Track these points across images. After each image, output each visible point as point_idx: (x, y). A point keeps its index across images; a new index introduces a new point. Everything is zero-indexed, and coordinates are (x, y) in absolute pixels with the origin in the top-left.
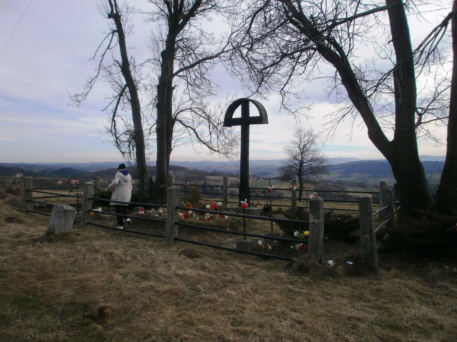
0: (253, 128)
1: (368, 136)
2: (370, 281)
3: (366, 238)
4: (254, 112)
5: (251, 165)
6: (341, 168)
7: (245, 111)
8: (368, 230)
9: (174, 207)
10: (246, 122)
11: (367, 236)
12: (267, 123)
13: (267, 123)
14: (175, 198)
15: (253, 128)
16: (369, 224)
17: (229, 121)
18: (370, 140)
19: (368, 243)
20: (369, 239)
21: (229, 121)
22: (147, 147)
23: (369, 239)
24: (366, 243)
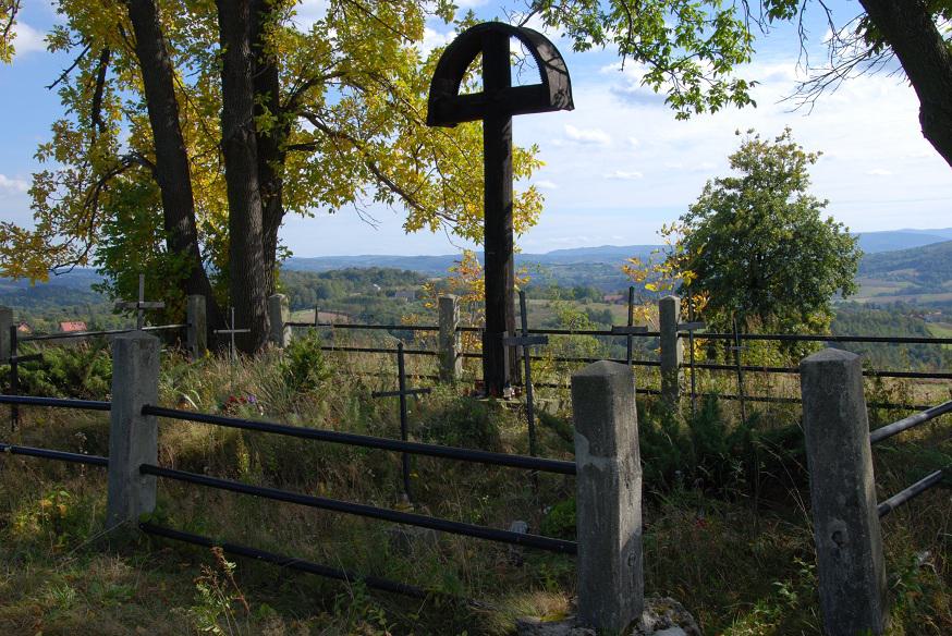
0: (525, 129)
1: (919, 127)
2: (39, 282)
3: (837, 534)
4: (524, 72)
5: (521, 276)
6: (912, 265)
7: (498, 68)
8: (842, 500)
9: (137, 407)
10: (502, 103)
11: (838, 523)
12: (570, 106)
13: (570, 106)
14: (137, 374)
15: (525, 129)
16: (846, 472)
17: (446, 109)
18: (927, 143)
19: (846, 555)
20: (846, 539)
21: (446, 109)
22: (519, 166)
23: (846, 539)
24: (837, 553)
